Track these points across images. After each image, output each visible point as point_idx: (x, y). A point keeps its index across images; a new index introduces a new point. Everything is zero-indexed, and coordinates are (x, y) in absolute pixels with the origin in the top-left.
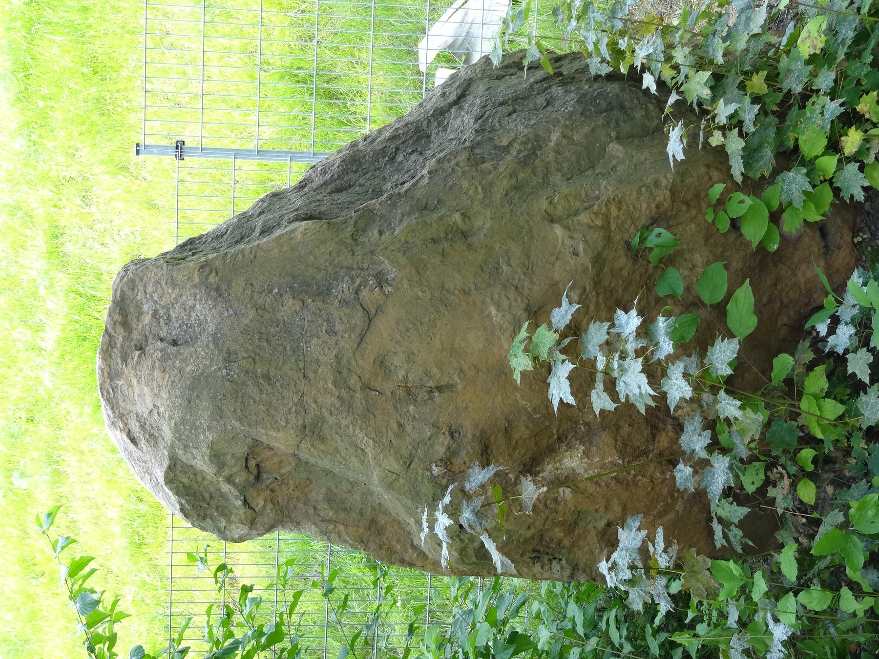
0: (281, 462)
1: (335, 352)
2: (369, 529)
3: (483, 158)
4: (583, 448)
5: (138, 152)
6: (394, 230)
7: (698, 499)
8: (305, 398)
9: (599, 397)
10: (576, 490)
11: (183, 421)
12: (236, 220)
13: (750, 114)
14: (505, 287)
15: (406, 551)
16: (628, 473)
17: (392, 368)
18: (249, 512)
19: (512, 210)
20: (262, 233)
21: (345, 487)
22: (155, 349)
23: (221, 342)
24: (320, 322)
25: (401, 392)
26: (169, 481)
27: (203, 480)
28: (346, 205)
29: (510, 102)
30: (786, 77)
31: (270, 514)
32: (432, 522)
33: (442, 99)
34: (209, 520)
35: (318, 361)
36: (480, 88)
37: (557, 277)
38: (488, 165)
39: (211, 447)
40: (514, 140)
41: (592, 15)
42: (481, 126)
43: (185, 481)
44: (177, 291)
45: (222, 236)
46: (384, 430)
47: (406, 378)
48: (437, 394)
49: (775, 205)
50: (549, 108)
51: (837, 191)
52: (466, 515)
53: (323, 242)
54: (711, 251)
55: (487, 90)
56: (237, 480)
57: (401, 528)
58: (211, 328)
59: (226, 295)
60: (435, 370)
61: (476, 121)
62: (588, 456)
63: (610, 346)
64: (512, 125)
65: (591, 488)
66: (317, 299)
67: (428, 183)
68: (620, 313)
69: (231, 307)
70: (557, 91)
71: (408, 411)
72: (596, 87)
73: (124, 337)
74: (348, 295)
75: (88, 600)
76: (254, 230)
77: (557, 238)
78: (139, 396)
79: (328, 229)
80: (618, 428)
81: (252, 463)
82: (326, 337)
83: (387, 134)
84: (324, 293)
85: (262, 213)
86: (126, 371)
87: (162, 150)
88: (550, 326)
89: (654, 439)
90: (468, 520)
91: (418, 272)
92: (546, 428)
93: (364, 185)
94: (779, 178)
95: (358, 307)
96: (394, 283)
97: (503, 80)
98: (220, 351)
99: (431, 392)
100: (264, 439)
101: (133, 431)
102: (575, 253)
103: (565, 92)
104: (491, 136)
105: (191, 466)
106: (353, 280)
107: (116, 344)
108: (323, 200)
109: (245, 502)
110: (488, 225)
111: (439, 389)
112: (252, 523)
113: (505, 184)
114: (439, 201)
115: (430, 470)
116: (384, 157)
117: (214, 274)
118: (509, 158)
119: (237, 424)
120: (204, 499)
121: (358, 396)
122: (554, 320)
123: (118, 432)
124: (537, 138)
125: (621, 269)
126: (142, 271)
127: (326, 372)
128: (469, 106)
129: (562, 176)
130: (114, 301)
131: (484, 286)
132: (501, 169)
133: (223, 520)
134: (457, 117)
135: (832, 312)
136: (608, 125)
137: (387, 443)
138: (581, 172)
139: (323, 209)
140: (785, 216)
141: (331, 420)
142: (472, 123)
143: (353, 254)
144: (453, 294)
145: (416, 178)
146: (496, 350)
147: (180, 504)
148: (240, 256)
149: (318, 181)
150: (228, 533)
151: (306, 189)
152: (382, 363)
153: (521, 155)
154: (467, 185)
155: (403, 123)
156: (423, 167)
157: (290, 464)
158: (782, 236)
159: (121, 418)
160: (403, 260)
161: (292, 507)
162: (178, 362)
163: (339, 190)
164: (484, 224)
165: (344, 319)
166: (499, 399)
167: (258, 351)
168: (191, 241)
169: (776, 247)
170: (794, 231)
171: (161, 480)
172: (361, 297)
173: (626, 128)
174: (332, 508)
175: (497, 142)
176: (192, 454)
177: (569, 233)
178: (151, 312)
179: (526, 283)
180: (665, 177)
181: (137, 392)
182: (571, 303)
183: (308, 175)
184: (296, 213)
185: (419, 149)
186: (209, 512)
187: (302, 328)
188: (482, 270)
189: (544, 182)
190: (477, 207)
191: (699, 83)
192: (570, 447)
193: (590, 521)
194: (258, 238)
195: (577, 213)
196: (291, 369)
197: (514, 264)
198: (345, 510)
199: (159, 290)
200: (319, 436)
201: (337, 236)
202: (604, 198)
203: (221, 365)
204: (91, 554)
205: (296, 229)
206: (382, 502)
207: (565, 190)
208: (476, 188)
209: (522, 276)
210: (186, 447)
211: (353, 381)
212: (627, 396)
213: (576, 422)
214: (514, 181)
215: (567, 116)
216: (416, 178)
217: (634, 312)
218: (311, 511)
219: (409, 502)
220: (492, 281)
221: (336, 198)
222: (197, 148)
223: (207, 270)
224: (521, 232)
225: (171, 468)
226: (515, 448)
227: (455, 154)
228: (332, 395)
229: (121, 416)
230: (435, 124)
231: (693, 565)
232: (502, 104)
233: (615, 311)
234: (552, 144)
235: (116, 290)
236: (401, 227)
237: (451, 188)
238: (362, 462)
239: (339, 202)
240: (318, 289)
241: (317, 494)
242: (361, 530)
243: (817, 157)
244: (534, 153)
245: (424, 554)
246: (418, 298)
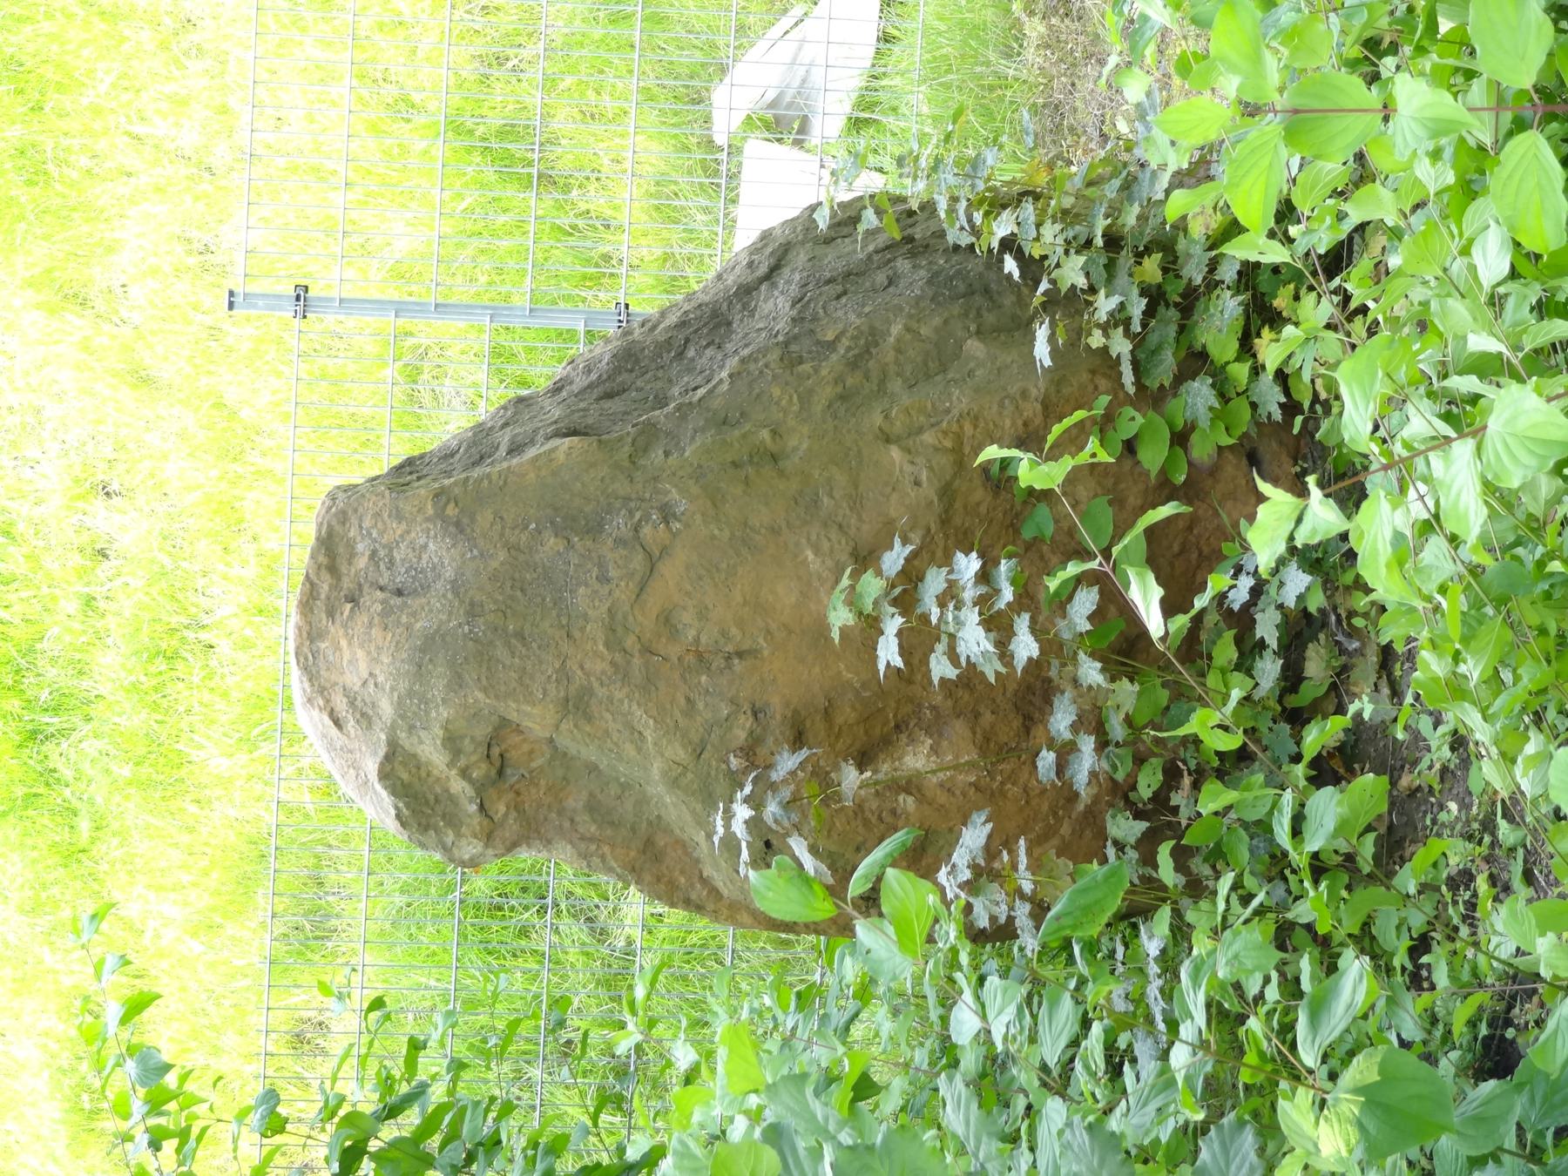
0: (531, 752)
1: (608, 605)
2: (644, 852)
3: (801, 357)
4: (930, 741)
5: (231, 306)
6: (684, 451)
7: (1092, 820)
8: (569, 663)
9: (939, 662)
10: (922, 798)
11: (411, 693)
13: (1137, 307)
14: (825, 525)
15: (692, 886)
16: (993, 779)
17: (680, 627)
18: (486, 822)
19: (836, 427)
20: (511, 452)
21: (614, 790)
22: (373, 601)
23: (463, 590)
24: (589, 566)
25: (690, 659)
26: (384, 776)
27: (428, 775)
28: (620, 416)
29: (840, 279)
30: (1186, 262)
31: (512, 827)
32: (729, 816)
33: (749, 271)
34: (432, 833)
35: (585, 617)
36: (800, 258)
37: (893, 514)
38: (806, 367)
40: (843, 333)
41: (942, 176)
42: (799, 313)
43: (405, 776)
44: (404, 526)
45: (452, 455)
46: (668, 706)
47: (697, 640)
48: (736, 661)
49: (1180, 424)
50: (891, 289)
51: (1254, 406)
52: (772, 809)
53: (593, 465)
54: (1099, 483)
55: (810, 260)
56: (474, 775)
57: (686, 853)
58: (449, 573)
59: (469, 531)
60: (734, 631)
61: (793, 306)
62: (936, 753)
63: (951, 595)
64: (840, 313)
65: (942, 798)
66: (586, 537)
67: (729, 390)
68: (960, 555)
69: (476, 547)
70: (903, 265)
71: (699, 683)
72: (953, 263)
73: (331, 586)
75: (152, 1062)
76: (497, 448)
77: (894, 463)
78: (350, 662)
79: (599, 448)
80: (977, 716)
81: (496, 751)
82: (597, 586)
83: (672, 319)
84: (594, 529)
85: (506, 425)
86: (332, 630)
87: (273, 301)
88: (879, 573)
89: (1028, 733)
90: (774, 814)
91: (715, 505)
92: (879, 710)
93: (642, 389)
94: (1183, 389)
95: (638, 547)
96: (683, 518)
97: (833, 244)
98: (462, 602)
99: (728, 658)
100: (514, 716)
101: (337, 709)
102: (917, 483)
103: (914, 267)
104: (812, 327)
105: (414, 756)
106: (631, 513)
107: (319, 594)
108: (588, 410)
109: (482, 807)
110: (805, 446)
111: (740, 655)
112: (488, 838)
113: (827, 392)
114: (742, 414)
115: (727, 762)
116: (669, 352)
117: (452, 505)
118: (834, 357)
119: (480, 695)
120: (427, 802)
122: (885, 567)
123: (315, 713)
124: (873, 331)
125: (978, 504)
126: (357, 499)
127: (595, 630)
128: (785, 283)
129: (904, 382)
130: (318, 539)
131: (798, 523)
132: (824, 372)
133: (450, 832)
134: (769, 298)
135: (1236, 560)
136: (966, 315)
137: (672, 724)
138: (928, 377)
139: (590, 421)
140: (1195, 438)
141: (601, 692)
142: (787, 309)
143: (631, 481)
144: (759, 533)
145: (714, 382)
146: (813, 606)
147: (397, 808)
148: (486, 482)
149: (580, 382)
150: (455, 851)
151: (564, 393)
152: (667, 620)
153: (850, 354)
154: (779, 393)
155: (694, 304)
156: (722, 367)
157: (543, 755)
158: (1190, 464)
159: (322, 693)
160: (695, 490)
161: (542, 817)
162: (404, 616)
163: (609, 396)
164: (800, 443)
165: (620, 562)
166: (817, 670)
167: (509, 602)
168: (410, 462)
169: (1183, 478)
170: (1206, 458)
172: (641, 535)
173: (990, 318)
174: (594, 821)
175: (819, 336)
176: (419, 737)
177: (908, 457)
178: (367, 553)
179: (853, 521)
180: (1036, 386)
181: (347, 656)
182: (904, 545)
183: (565, 373)
184: (554, 427)
185: (717, 341)
186: (432, 821)
187: (566, 573)
188: (796, 503)
189: (879, 391)
190: (791, 423)
191: (1073, 270)
192: (912, 740)
193: (943, 847)
194: (505, 459)
195: (921, 430)
196: (551, 626)
197: (837, 494)
198: (612, 824)
199: (380, 525)
200: (585, 712)
201: (611, 457)
202: (955, 412)
204: (156, 989)
205: (557, 448)
206: (662, 814)
207: (905, 400)
208: (791, 397)
209: (848, 512)
210: (411, 728)
211: (630, 642)
212: (968, 657)
213: (920, 705)
214: (839, 389)
215: (913, 303)
216: (714, 382)
217: (974, 555)
218: (567, 824)
219: (699, 807)
220: (808, 518)
221: (606, 406)
222: (331, 300)
223: (444, 499)
224: (847, 455)
225: (389, 758)
226: (838, 737)
227: (764, 351)
228: (603, 659)
229: (322, 690)
230: (739, 306)
231: (1052, 870)
232: (829, 282)
233: (955, 553)
234: (892, 339)
235: (322, 523)
236: (694, 447)
237: (758, 396)
238: (639, 750)
239: (610, 412)
240: (586, 524)
241: (575, 801)
242: (633, 854)
243: (1227, 363)
244: (868, 351)
245: (718, 891)
246: (713, 537)
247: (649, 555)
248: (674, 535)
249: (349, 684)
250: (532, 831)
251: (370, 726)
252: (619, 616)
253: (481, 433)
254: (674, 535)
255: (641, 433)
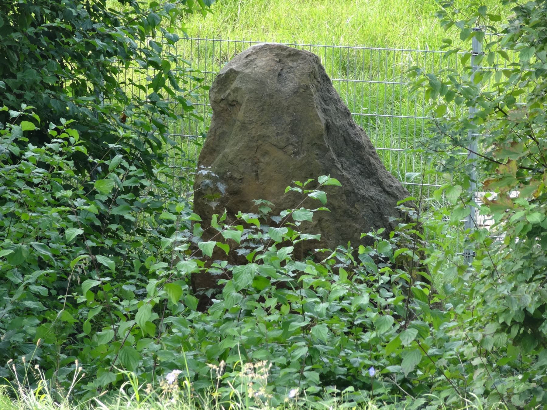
11: (250, 78)
12: (336, 98)
14: (294, 201)
25: (256, 160)
26: (231, 70)
31: (218, 109)
38: (344, 197)
39: (240, 88)
40: (357, 210)
43: (231, 77)
45: (329, 92)
47: (261, 162)
55: (389, 204)
58: (283, 89)
60: (263, 173)
61: (370, 196)
64: (365, 210)
74: (291, 141)
81: (235, 103)
82: (276, 132)
98: (273, 93)
99: (256, 171)
109: (222, 100)
110: (11, 70)
111: (257, 175)
115: (228, 171)
119: (247, 98)
120: (224, 83)
121: (255, 144)
132: (343, 203)
141: (247, 133)
160: (304, 162)
163: (345, 140)
171: (232, 67)
198: (219, 139)
202: (328, 241)
203: (268, 93)
210: (241, 78)
211: (260, 142)
214: (337, 207)
218: (219, 125)
219: (218, 163)
223: (305, 88)
228: (256, 134)
229: (256, 52)
230: (374, 181)
232: (379, 208)
234: (354, 224)
238: (232, 145)
241: (225, 128)
244: (350, 217)
246: (289, 167)
247: (284, 148)
248: (290, 155)
249: (257, 60)
250: (218, 115)
251: (244, 66)
252: (267, 139)
253: (337, 101)
254: (290, 155)
255: (325, 147)
